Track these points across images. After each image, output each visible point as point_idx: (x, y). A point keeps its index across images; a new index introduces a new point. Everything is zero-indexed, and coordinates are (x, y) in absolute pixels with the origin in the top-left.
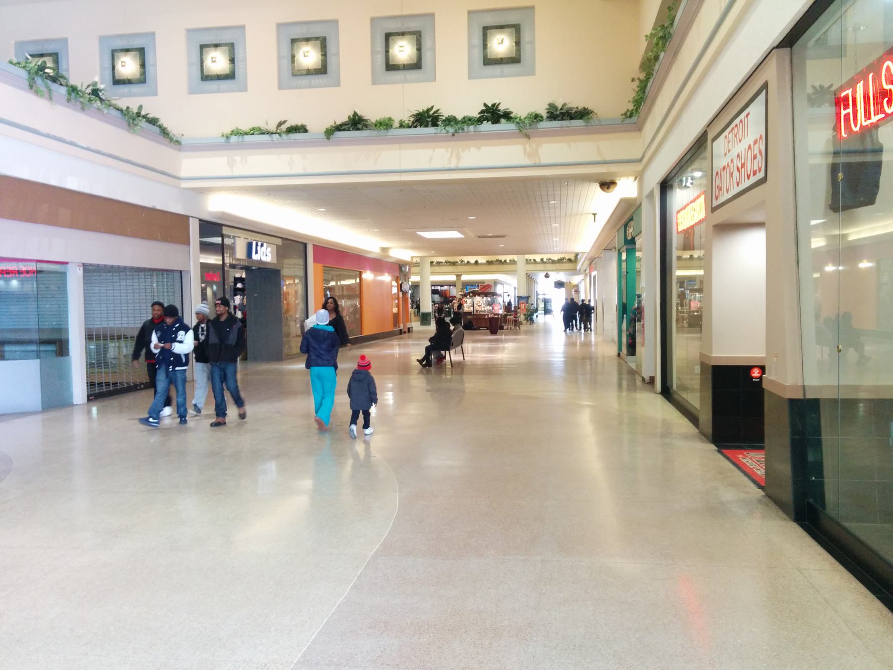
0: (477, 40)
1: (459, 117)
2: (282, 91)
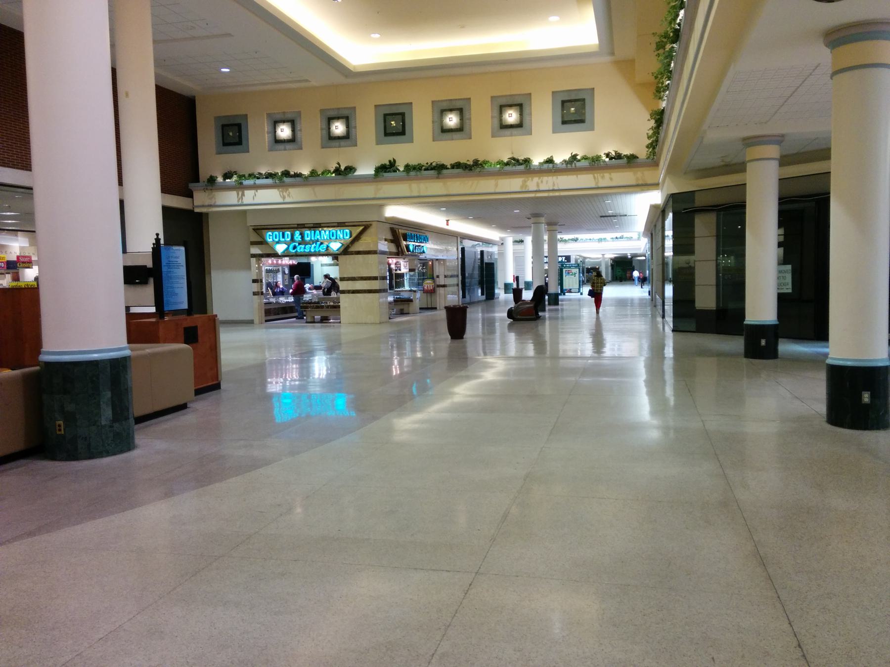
0: (496, 114)
1: (292, 173)
2: (33, 167)
